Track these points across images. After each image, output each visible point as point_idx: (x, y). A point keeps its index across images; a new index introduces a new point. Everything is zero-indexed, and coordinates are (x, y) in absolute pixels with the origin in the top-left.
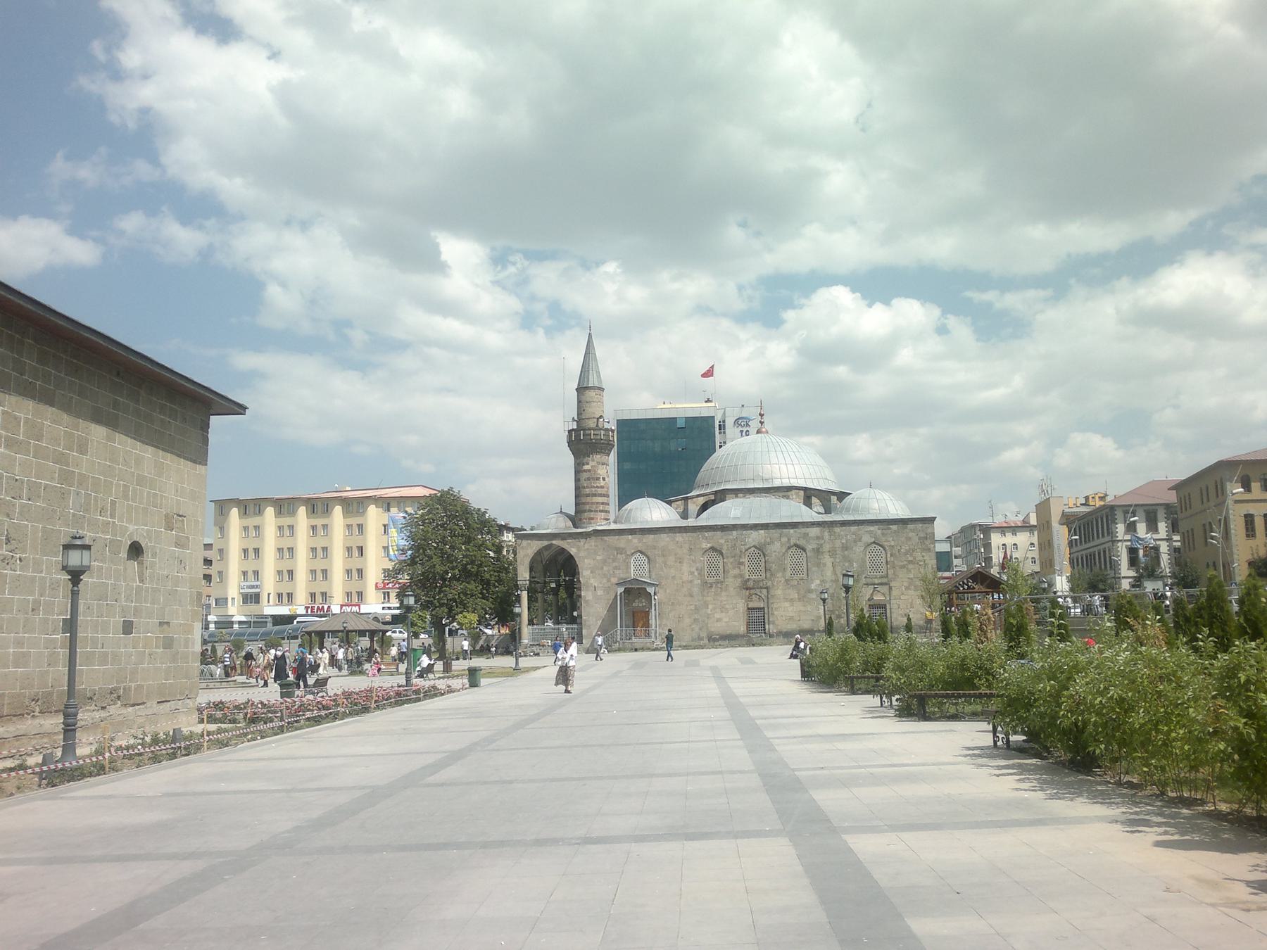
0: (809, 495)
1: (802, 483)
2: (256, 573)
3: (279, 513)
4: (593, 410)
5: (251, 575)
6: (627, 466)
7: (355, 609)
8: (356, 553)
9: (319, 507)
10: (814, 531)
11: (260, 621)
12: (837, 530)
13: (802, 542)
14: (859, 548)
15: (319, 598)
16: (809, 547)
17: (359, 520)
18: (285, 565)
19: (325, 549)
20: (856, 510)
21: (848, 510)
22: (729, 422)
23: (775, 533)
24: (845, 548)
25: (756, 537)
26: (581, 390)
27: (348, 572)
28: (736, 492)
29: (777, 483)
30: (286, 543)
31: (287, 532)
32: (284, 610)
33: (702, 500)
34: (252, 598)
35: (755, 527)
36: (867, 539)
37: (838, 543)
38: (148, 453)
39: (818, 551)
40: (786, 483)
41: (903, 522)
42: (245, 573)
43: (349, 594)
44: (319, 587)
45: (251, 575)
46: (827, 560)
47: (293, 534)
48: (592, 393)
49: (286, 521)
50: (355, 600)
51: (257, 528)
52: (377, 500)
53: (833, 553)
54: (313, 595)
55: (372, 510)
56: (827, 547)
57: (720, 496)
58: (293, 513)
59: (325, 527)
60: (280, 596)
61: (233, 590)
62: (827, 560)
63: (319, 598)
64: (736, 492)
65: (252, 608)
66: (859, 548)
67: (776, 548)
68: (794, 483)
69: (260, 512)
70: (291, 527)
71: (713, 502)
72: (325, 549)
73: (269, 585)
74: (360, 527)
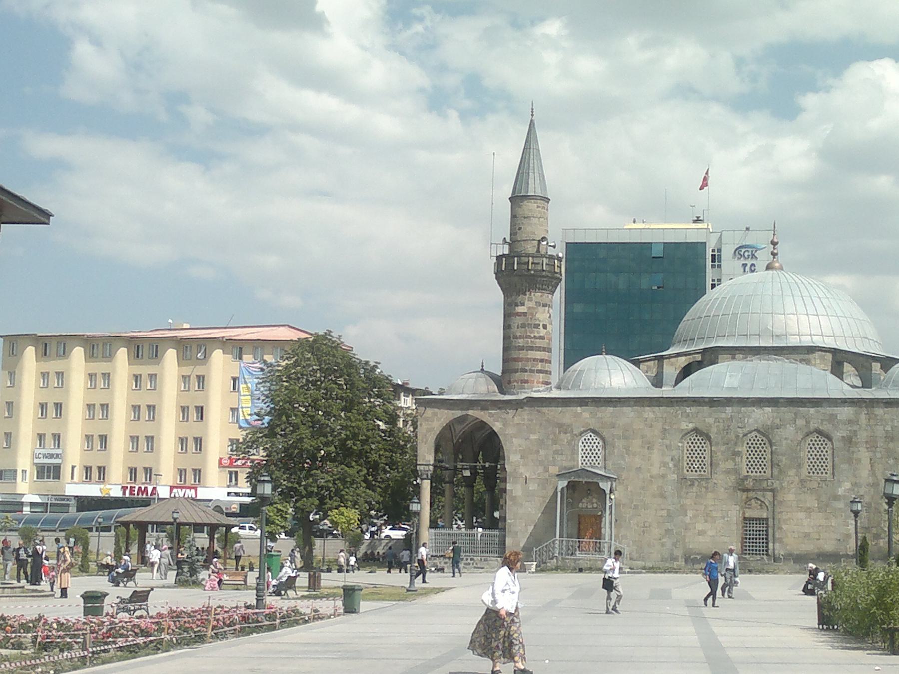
0: (839, 360)
2: (57, 438)
3: (91, 356)
4: (532, 229)
5: (49, 441)
7: (190, 493)
8: (193, 416)
9: (145, 349)
10: (845, 413)
11: (60, 504)
12: (879, 411)
16: (837, 435)
17: (200, 371)
18: (97, 429)
19: (151, 408)
22: (727, 252)
23: (787, 413)
27: (183, 441)
28: (733, 352)
29: (793, 341)
30: (98, 398)
32: (93, 490)
33: (683, 362)
34: (49, 471)
37: (879, 431)
39: (849, 441)
40: (806, 341)
42: (41, 437)
43: (182, 472)
44: (142, 461)
45: (49, 441)
46: (863, 455)
49: (100, 367)
50: (190, 480)
51: (60, 375)
52: (226, 344)
53: (871, 445)
54: (133, 472)
56: (862, 436)
57: (710, 357)
58: (110, 357)
59: (153, 377)
60: (88, 470)
62: (863, 455)
64: (733, 352)
65: (50, 484)
67: (788, 434)
68: (818, 342)
69: (65, 354)
71: (700, 365)
73: (74, 454)
74: (201, 379)
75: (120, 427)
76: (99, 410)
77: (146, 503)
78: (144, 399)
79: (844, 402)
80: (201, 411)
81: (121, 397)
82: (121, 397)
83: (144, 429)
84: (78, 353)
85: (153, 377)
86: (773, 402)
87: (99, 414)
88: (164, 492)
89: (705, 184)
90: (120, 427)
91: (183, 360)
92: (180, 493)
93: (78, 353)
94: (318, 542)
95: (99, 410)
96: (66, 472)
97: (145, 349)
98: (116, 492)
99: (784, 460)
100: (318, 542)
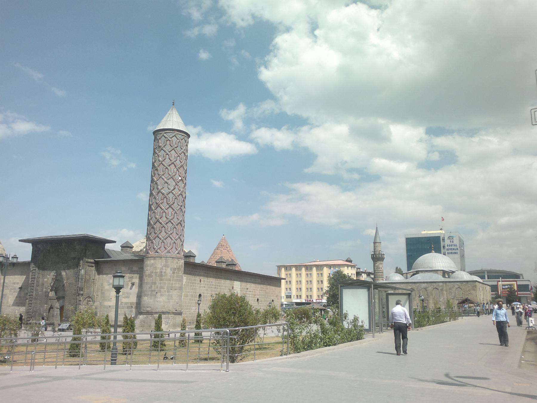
0: (444, 273)
1: (442, 269)
2: (290, 289)
3: (296, 270)
4: (378, 249)
5: (288, 289)
6: (410, 254)
7: (320, 301)
8: (320, 282)
9: (309, 268)
10: (441, 284)
11: (292, 304)
12: (448, 284)
13: (437, 287)
14: (454, 289)
15: (309, 297)
16: (440, 289)
17: (321, 272)
18: (299, 287)
19: (311, 281)
20: (454, 278)
21: (452, 278)
22: (446, 238)
23: (429, 284)
24: (450, 289)
25: (424, 285)
26: (375, 243)
27: (318, 289)
28: (422, 271)
29: (434, 269)
30: (299, 279)
31: (299, 276)
32: (298, 301)
33: (412, 273)
34: (288, 297)
35: (424, 283)
36: (456, 286)
37: (448, 288)
38: (274, 288)
39: (442, 290)
40: (437, 269)
41: (467, 282)
42: (287, 289)
43: (318, 296)
44: (309, 294)
45: (288, 289)
46: (445, 292)
47: (301, 276)
48: (377, 244)
49: (298, 272)
50: (320, 298)
51: (290, 274)
52: (327, 265)
53: (446, 291)
54: (307, 296)
55: (325, 269)
56: (444, 289)
57: (417, 272)
58: (301, 270)
59: (310, 274)
60: (297, 296)
61: (283, 294)
62: (445, 292)
63: (309, 297)
64: (422, 271)
65: (289, 300)
66: (454, 289)
67: (430, 289)
68: (440, 269)
69: (291, 270)
70: (300, 274)
71: (416, 274)
72: (311, 281)
73: (294, 293)
74: (322, 274)
75: (304, 286)
76: (299, 282)
77: (310, 304)
78: (309, 279)
79: (441, 282)
80: (322, 281)
81: (304, 279)
82: (304, 279)
83: (309, 286)
84: (294, 269)
85: (310, 274)
86: (427, 282)
87: (299, 283)
88: (314, 301)
89: (443, 220)
90: (304, 286)
91: (317, 270)
92: (318, 301)
93: (294, 269)
94: (119, 323)
95: (299, 282)
96: (292, 297)
97: (309, 268)
98: (304, 301)
99: (429, 294)
100: (119, 323)
